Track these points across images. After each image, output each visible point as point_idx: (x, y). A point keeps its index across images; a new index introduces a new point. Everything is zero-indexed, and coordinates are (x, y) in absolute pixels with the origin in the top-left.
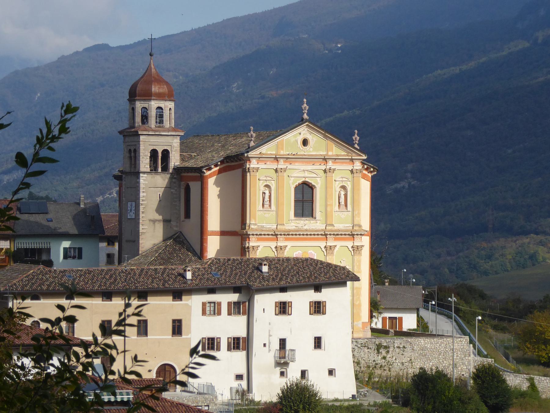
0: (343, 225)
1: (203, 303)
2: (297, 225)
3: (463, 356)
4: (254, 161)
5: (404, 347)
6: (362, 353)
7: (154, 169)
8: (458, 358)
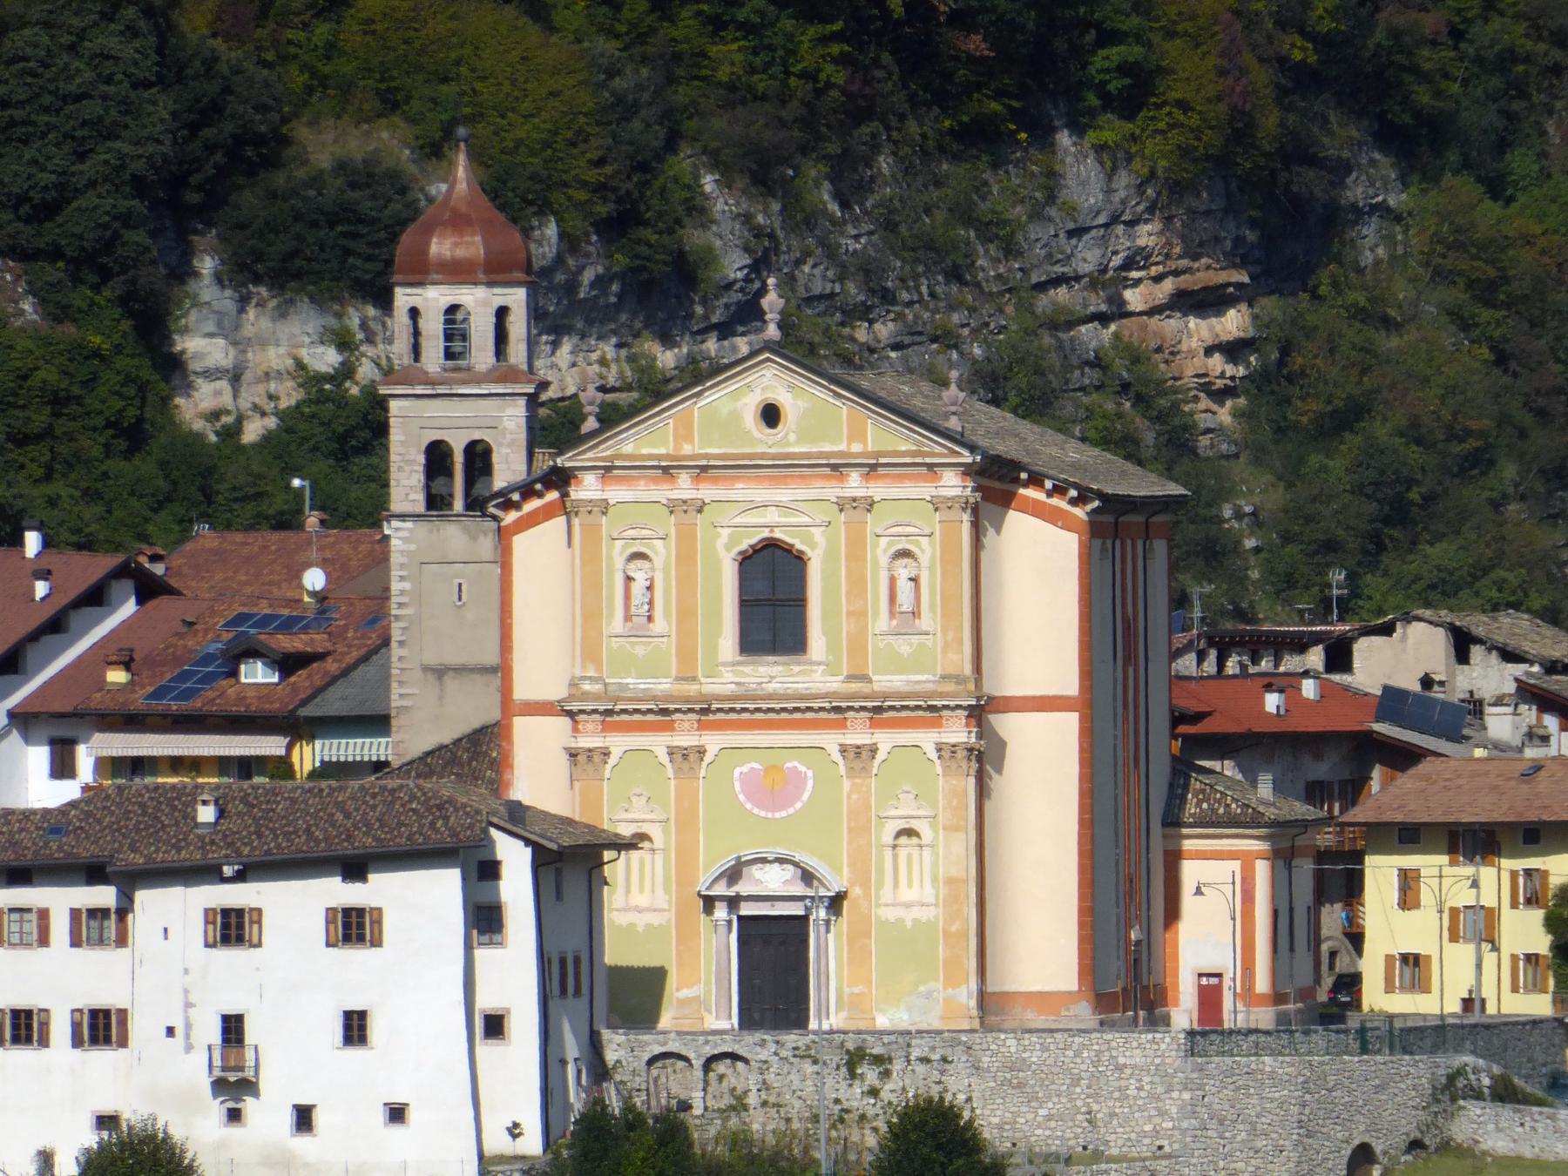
0: (904, 677)
1: (72, 910)
2: (742, 680)
3: (1160, 1089)
4: (590, 479)
5: (944, 1060)
6: (795, 1077)
7: (436, 502)
8: (1143, 1094)
